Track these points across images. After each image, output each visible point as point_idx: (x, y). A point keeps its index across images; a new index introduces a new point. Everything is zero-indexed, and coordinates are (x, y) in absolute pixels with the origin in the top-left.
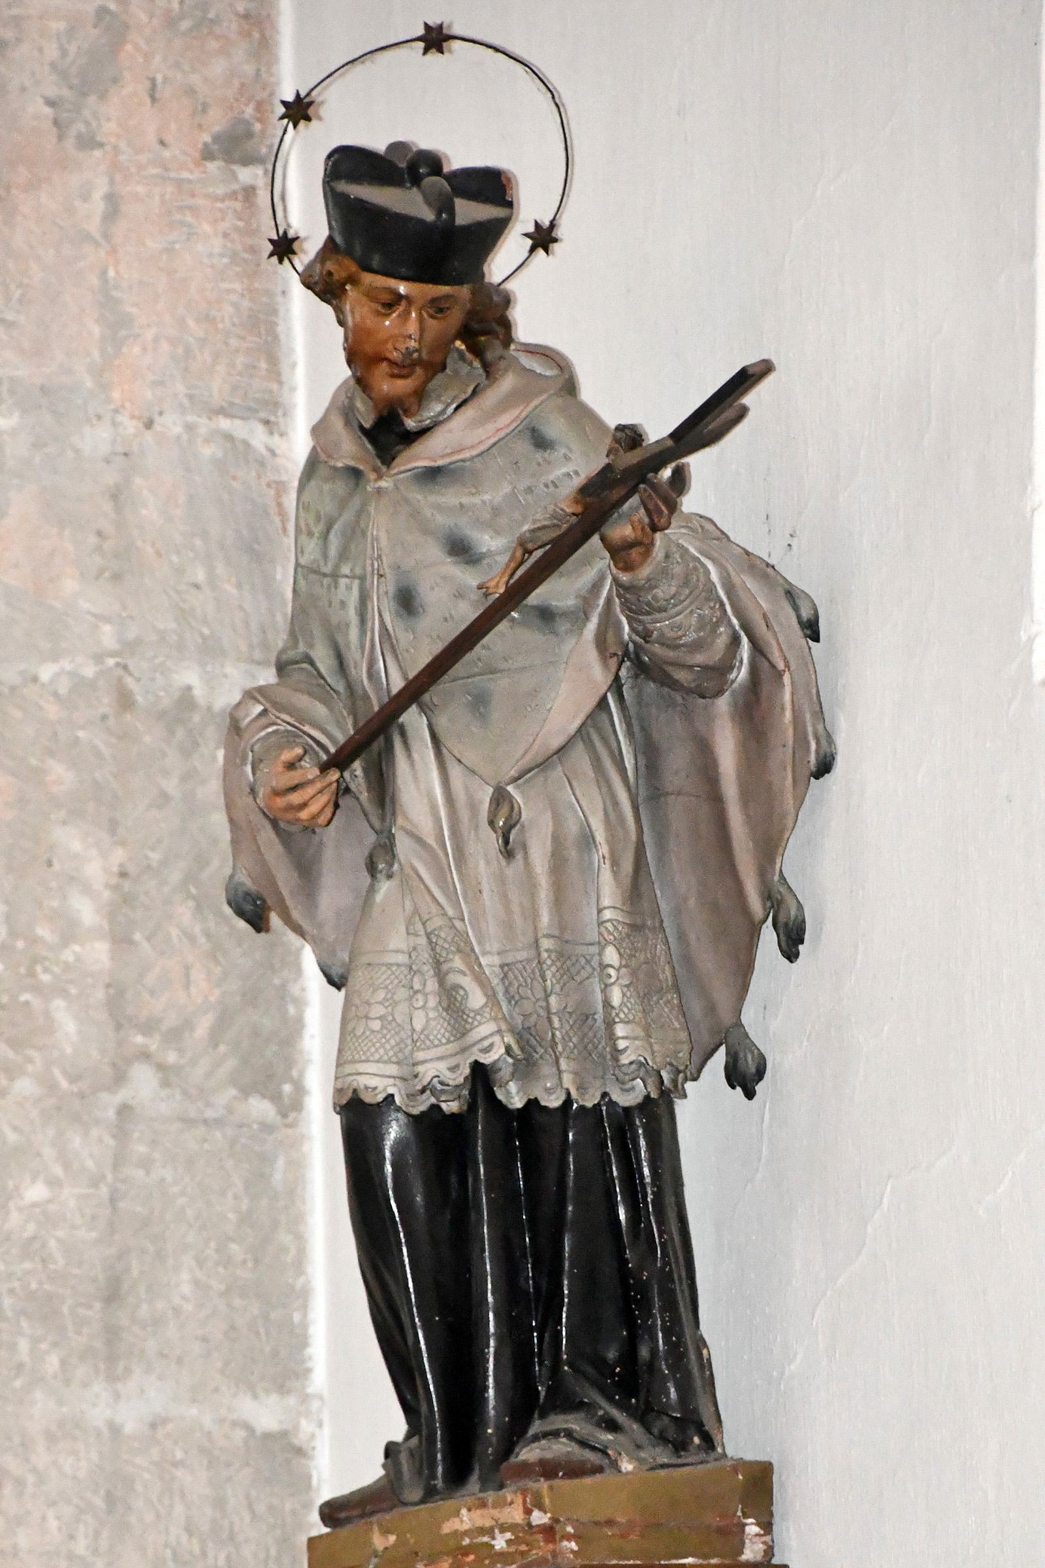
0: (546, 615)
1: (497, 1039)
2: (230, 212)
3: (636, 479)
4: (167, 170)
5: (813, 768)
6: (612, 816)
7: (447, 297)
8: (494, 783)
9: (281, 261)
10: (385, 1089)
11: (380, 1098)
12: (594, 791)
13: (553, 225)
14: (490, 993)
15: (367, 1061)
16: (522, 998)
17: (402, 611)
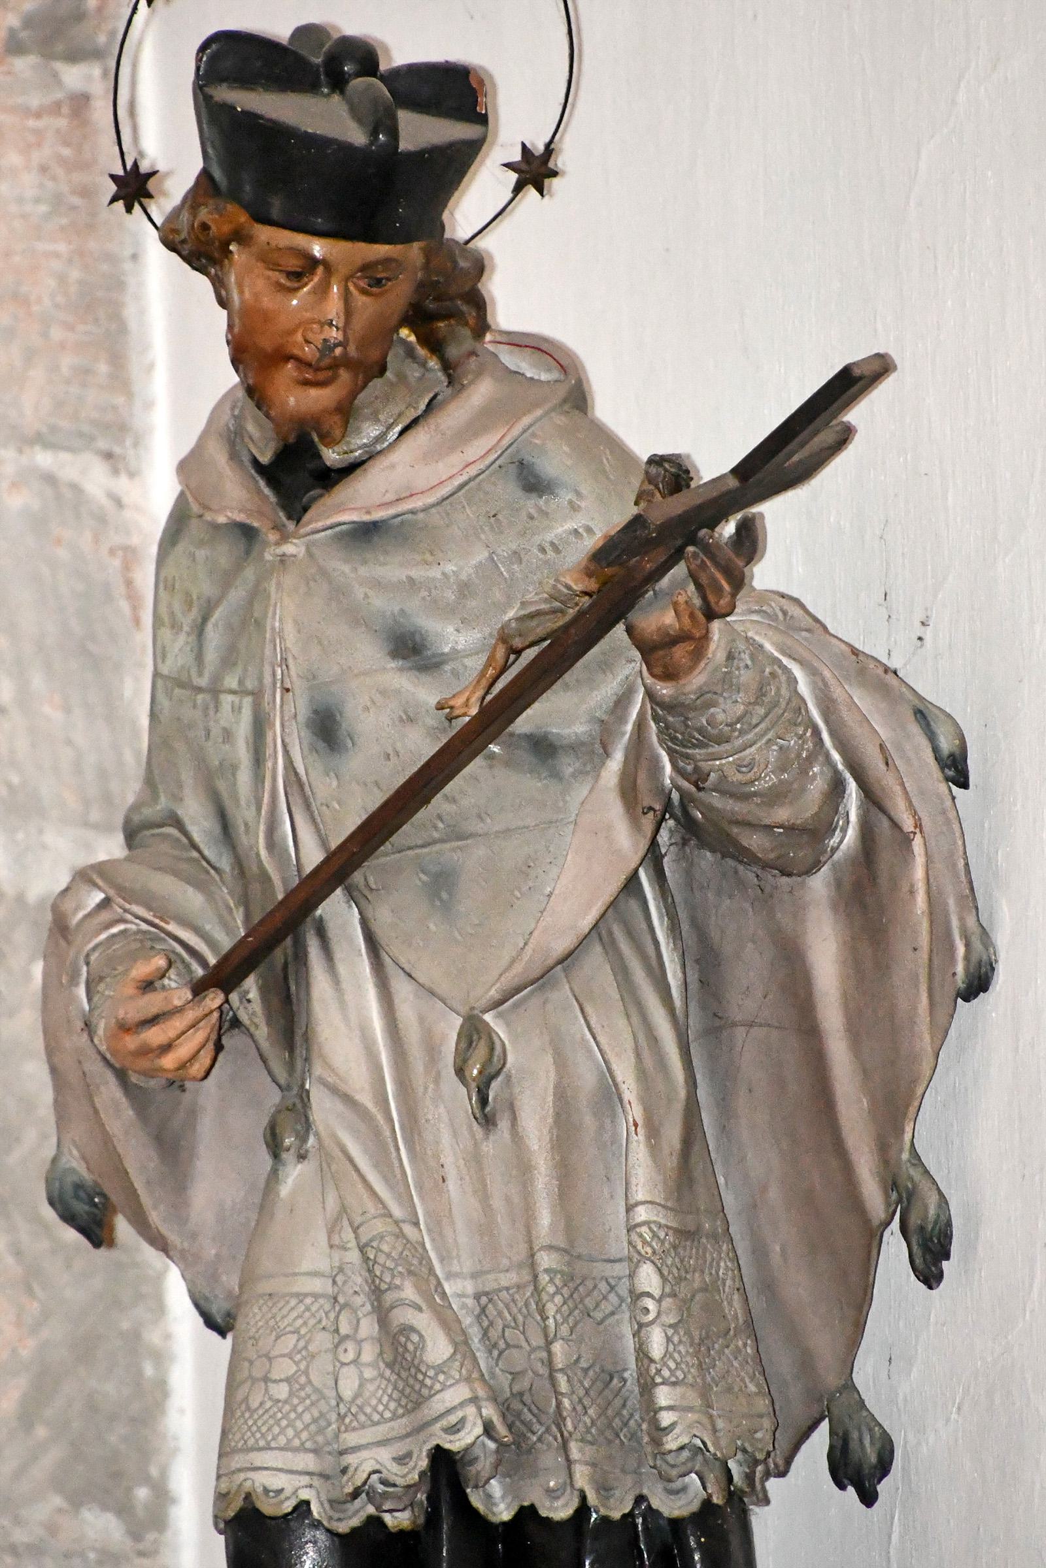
0: (543, 748)
1: (471, 1410)
3: (682, 538)
7: (387, 261)
8: (464, 1010)
9: (129, 209)
11: (288, 1507)
12: (621, 1023)
13: (549, 150)
15: (268, 1448)
16: (508, 1346)
17: (321, 745)
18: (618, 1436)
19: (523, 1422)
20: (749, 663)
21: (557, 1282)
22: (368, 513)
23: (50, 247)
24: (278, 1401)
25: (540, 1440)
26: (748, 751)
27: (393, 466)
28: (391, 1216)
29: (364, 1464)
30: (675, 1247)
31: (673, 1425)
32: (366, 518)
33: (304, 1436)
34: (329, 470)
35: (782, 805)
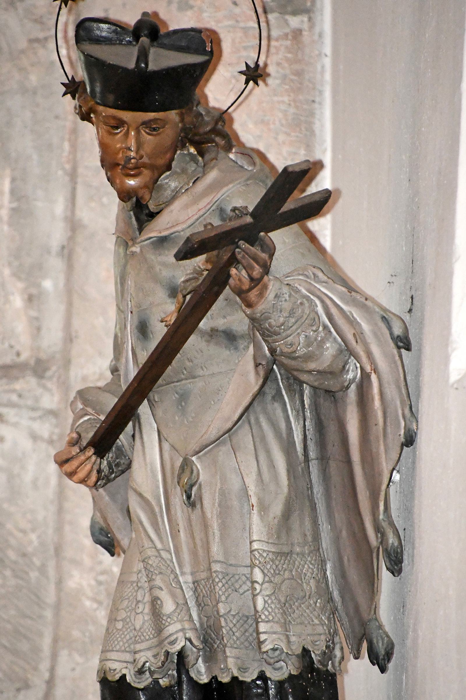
2: (283, 49)
4: (237, 21)
5: (403, 440)
6: (266, 476)
7: (155, 120)
10: (120, 671)
11: (117, 677)
14: (181, 602)
16: (205, 605)
17: (141, 336)
18: (251, 645)
19: (211, 639)
20: (288, 298)
21: (220, 576)
22: (160, 233)
23: (281, 99)
24: (118, 630)
25: (218, 646)
26: (289, 339)
27: (172, 211)
28: (155, 548)
29: (142, 658)
30: (273, 561)
31: (266, 640)
32: (159, 235)
33: (126, 645)
34: (153, 213)
35: (312, 362)
